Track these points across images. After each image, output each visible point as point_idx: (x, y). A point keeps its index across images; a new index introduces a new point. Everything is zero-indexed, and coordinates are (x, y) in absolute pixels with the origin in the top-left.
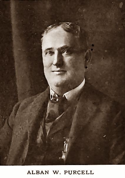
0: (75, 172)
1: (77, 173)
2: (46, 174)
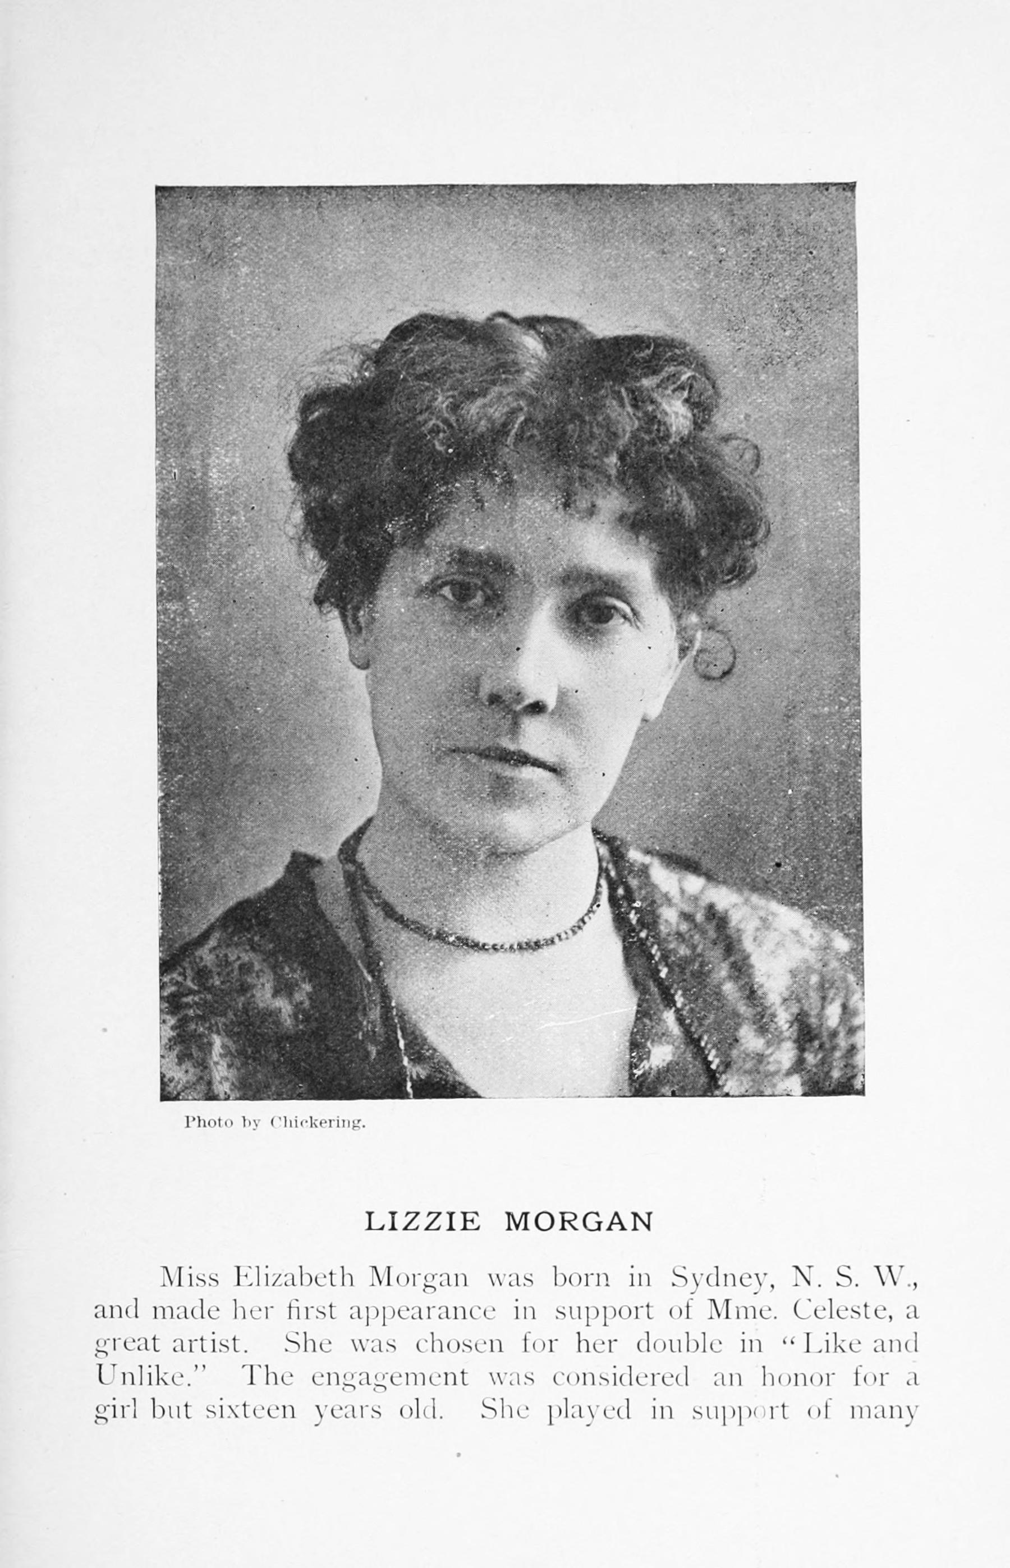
0: (568, 1217)
1: (578, 1223)
2: (635, 1229)
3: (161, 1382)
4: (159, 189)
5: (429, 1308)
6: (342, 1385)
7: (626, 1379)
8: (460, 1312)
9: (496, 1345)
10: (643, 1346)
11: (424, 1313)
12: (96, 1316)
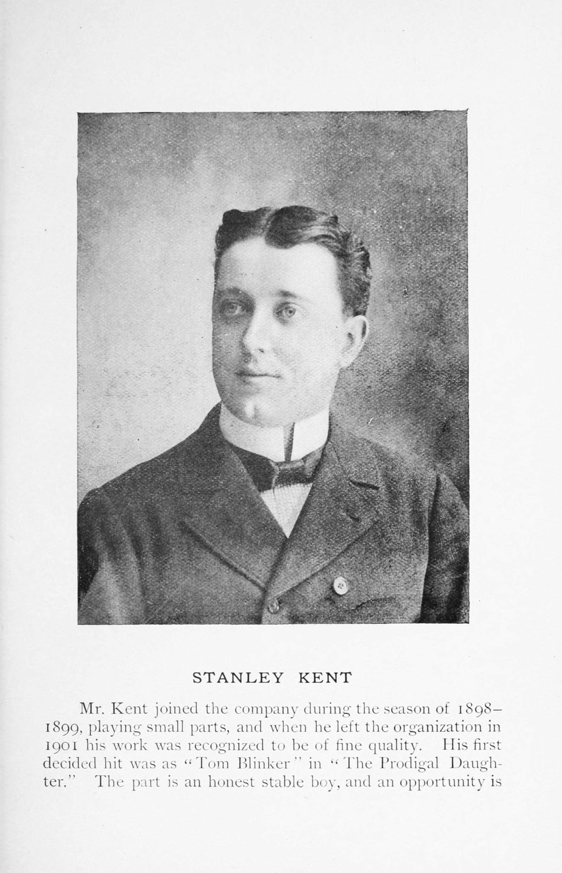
2: (233, 682)
3: (143, 748)
4: (81, 116)
5: (209, 726)
6: (218, 750)
7: (76, 765)
8: (358, 782)
9: (303, 728)
10: (308, 710)
11: (207, 728)
12: (238, 731)
